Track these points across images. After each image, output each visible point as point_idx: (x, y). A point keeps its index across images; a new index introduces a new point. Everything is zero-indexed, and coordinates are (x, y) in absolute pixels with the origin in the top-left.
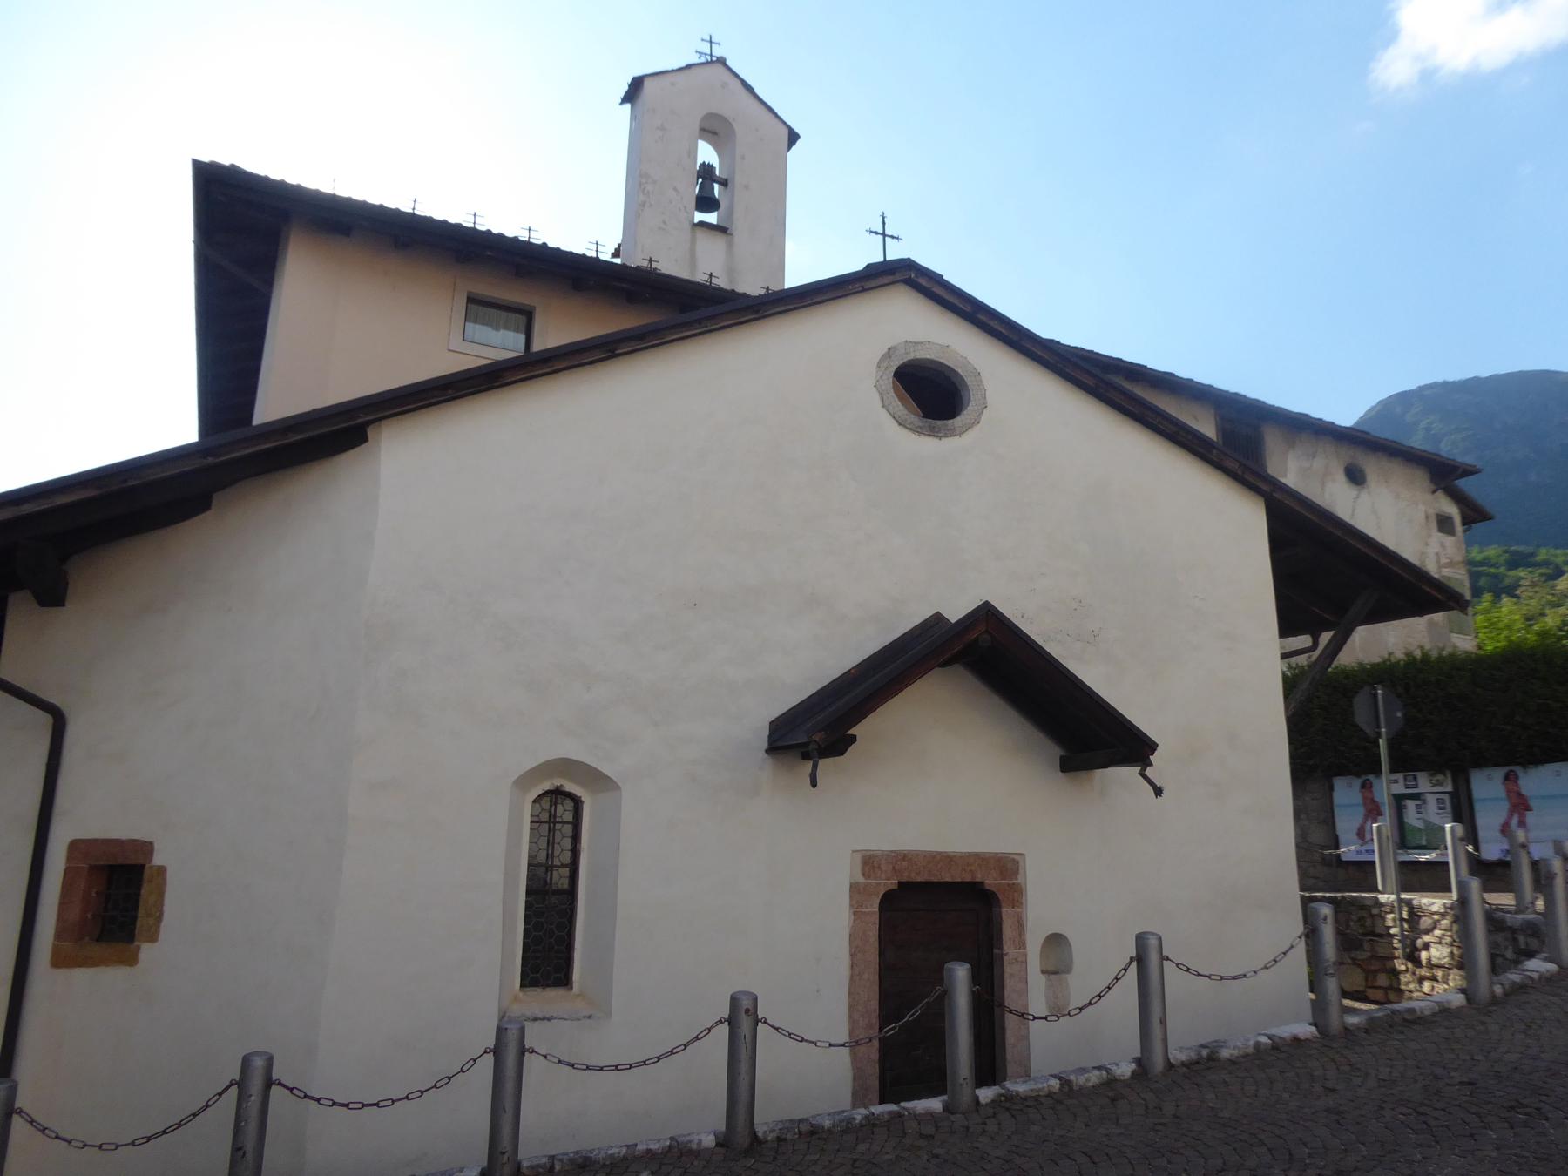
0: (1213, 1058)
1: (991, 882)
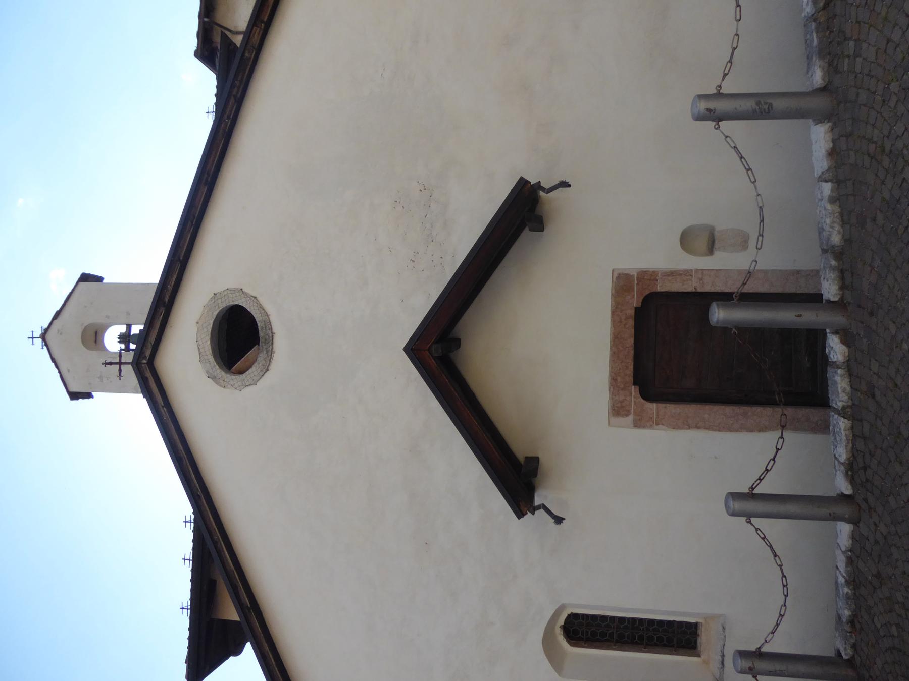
0: (839, 254)
1: (635, 301)
